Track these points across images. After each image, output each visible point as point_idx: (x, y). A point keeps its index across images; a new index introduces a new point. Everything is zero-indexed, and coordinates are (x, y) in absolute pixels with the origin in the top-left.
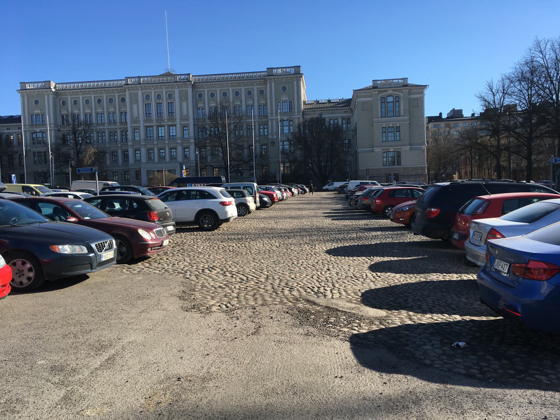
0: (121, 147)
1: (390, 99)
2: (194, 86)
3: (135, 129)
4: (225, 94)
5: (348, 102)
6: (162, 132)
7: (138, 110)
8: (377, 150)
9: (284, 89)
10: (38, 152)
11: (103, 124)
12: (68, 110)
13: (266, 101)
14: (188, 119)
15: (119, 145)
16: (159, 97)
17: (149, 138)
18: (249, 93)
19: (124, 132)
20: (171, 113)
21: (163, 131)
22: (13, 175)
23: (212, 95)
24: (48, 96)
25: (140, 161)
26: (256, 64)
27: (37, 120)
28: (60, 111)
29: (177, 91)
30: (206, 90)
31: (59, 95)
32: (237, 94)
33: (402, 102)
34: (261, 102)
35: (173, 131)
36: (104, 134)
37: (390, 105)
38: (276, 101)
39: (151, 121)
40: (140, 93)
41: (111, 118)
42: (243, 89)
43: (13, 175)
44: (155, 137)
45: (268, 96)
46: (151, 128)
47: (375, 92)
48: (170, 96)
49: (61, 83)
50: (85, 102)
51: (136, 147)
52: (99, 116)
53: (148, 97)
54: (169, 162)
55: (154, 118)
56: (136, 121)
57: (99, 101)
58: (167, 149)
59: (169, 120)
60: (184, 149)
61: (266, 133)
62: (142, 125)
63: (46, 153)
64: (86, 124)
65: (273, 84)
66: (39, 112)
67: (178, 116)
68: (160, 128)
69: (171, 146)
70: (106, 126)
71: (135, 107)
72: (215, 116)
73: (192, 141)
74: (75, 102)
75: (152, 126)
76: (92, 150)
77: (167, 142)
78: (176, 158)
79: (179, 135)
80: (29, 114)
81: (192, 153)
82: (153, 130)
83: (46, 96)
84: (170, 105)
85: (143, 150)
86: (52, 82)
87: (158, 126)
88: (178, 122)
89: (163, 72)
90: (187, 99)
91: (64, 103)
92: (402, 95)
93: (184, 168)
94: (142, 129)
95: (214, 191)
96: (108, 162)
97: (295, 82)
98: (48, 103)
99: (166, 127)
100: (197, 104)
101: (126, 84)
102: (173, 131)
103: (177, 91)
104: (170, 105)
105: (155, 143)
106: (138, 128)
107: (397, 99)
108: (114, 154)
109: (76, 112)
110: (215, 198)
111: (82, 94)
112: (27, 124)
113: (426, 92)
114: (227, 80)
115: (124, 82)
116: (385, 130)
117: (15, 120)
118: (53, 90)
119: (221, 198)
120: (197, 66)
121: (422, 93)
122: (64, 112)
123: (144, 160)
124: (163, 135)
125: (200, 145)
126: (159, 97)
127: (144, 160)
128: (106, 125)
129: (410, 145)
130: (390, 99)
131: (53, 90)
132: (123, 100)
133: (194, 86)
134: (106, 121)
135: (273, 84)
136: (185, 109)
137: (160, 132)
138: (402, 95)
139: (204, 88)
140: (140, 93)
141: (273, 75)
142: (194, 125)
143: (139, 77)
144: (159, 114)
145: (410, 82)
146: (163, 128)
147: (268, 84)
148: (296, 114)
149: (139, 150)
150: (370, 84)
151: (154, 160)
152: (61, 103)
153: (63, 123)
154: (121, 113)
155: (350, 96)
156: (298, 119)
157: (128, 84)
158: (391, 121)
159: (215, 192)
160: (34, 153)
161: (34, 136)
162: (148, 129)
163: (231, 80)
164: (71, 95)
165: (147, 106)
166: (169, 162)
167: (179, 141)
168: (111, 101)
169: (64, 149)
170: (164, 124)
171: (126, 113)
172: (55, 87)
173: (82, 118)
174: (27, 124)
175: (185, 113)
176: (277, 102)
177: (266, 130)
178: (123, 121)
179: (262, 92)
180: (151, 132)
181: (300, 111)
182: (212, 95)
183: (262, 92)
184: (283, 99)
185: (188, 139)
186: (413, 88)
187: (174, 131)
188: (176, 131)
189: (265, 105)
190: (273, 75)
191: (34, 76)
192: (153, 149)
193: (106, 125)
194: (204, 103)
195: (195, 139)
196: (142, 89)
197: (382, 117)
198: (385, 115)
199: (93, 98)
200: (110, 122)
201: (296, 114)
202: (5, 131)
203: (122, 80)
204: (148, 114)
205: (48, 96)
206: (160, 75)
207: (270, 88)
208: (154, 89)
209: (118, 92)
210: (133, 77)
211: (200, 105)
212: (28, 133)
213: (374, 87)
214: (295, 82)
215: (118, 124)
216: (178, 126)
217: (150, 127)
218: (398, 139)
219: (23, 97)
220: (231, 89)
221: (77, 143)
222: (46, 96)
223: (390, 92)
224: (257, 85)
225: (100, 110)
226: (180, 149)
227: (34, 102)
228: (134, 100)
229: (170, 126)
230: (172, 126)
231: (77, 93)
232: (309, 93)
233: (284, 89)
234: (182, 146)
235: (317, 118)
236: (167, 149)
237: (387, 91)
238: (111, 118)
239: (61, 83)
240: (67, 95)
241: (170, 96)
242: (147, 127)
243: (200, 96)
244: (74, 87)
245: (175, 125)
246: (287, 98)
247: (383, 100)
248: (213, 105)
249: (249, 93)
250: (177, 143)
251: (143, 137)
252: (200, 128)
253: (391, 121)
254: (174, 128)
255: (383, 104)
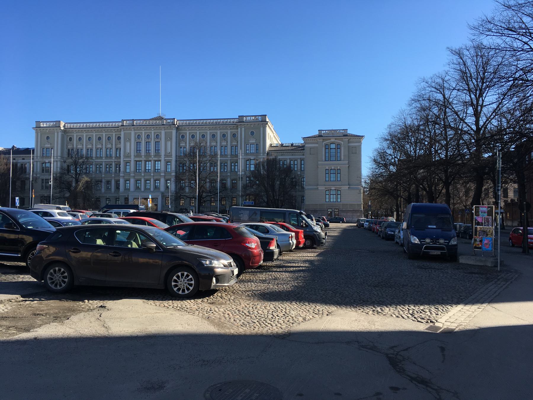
0: (115, 177)
1: (333, 146)
2: (178, 129)
3: (127, 163)
4: (203, 136)
5: (301, 148)
6: (149, 166)
7: (130, 147)
8: (321, 188)
9: (252, 133)
10: (46, 180)
11: (101, 158)
12: (73, 145)
13: (237, 142)
14: (171, 156)
15: (113, 175)
16: (148, 136)
17: (138, 171)
18: (224, 136)
19: (118, 165)
20: (157, 151)
21: (150, 165)
22: (17, 198)
23: (193, 136)
24: (58, 133)
25: (129, 189)
26: (229, 111)
27: (46, 152)
28: (67, 146)
29: (163, 132)
30: (188, 132)
31: (68, 133)
32: (214, 136)
33: (342, 149)
34: (234, 144)
35: (158, 166)
36: (91, 166)
37: (333, 151)
38: (245, 143)
39: (141, 156)
40: (133, 133)
41: (108, 153)
42: (219, 132)
43: (17, 198)
44: (143, 170)
45: (239, 139)
46: (140, 163)
47: (320, 140)
48: (157, 136)
49: (69, 123)
50: (87, 139)
51: (126, 178)
52: (108, 150)
53: (139, 137)
54: (143, 192)
55: (143, 154)
56: (129, 156)
57: (100, 139)
58: (152, 180)
59: (155, 156)
60: (167, 180)
61: (236, 170)
62: (133, 159)
63: (48, 181)
64: (87, 158)
65: (243, 129)
66: (49, 146)
67: (163, 153)
68: (147, 163)
69: (146, 177)
70: (104, 160)
71: (128, 144)
72: (192, 154)
73: (174, 174)
74: (80, 139)
75: (141, 161)
76: (85, 179)
77: (152, 174)
78: (159, 189)
79: (163, 169)
80: (41, 147)
81: (172, 186)
82: (141, 164)
83: (56, 134)
84: (157, 143)
85: (132, 181)
86: (62, 122)
87: (146, 161)
88: (162, 158)
89: (155, 116)
90: (171, 139)
91: (71, 139)
92: (342, 143)
93: (150, 197)
94: (132, 163)
95: (54, 213)
96: (103, 190)
97: (262, 129)
98: (57, 139)
99: (152, 162)
100: (179, 144)
101: (122, 126)
102: (158, 166)
103: (163, 132)
104: (157, 143)
105: (143, 175)
106: (129, 162)
107: (338, 147)
108: (108, 182)
109: (80, 147)
110: (53, 216)
111: (86, 133)
112: (39, 155)
113: (364, 142)
114: (206, 124)
115: (120, 124)
116: (328, 172)
117: (27, 151)
118: (62, 128)
119: (56, 216)
120: (181, 112)
121: (360, 142)
122: (70, 147)
123: (132, 188)
124: (150, 168)
125: (178, 179)
126: (148, 136)
127: (132, 188)
128: (104, 158)
129: (349, 185)
130: (333, 146)
131: (62, 128)
132: (119, 138)
133: (178, 129)
134: (104, 156)
135: (243, 129)
136: (169, 148)
137: (147, 165)
138: (342, 143)
139: (186, 130)
140: (133, 133)
141: (243, 122)
142: (176, 161)
143: (133, 120)
144: (148, 151)
145: (349, 132)
146: (150, 163)
147: (239, 129)
148: (262, 154)
149: (129, 180)
150: (317, 133)
151: (140, 189)
152: (68, 139)
153: (68, 156)
154: (117, 149)
155: (299, 141)
156: (262, 158)
157: (123, 126)
158: (333, 165)
159: (54, 213)
160: (43, 180)
161: (44, 165)
162: (138, 163)
163: (210, 124)
164: (76, 133)
165: (138, 144)
166: (143, 192)
167: (152, 174)
168: (109, 138)
169: (67, 178)
170: (141, 159)
171: (120, 149)
172: (64, 126)
173: (84, 152)
174: (39, 155)
175: (169, 150)
176: (246, 144)
177: (236, 167)
178: (118, 155)
179: (234, 135)
180: (140, 166)
181: (265, 153)
182: (193, 136)
183: (234, 135)
184: (251, 142)
185: (170, 173)
186: (352, 138)
187: (159, 165)
188: (160, 166)
189: (237, 146)
190: (243, 122)
191: (47, 117)
192: (140, 180)
193: (104, 158)
194: (186, 143)
195: (176, 173)
196: (134, 130)
197: (326, 160)
198: (328, 159)
199: (104, 136)
200: (107, 157)
201: (262, 154)
202: (19, 161)
203: (119, 122)
204: (138, 151)
205: (58, 133)
206: (152, 119)
207: (241, 132)
208: (145, 130)
209: (115, 132)
210: (128, 120)
211: (182, 144)
212: (39, 163)
213: (320, 136)
214: (262, 129)
215: (114, 158)
216: (163, 162)
217: (139, 161)
218: (339, 179)
219: (37, 133)
220: (208, 132)
221: (76, 174)
222: (56, 134)
223: (333, 140)
224: (231, 129)
225: (99, 146)
226: (162, 180)
227: (46, 138)
228: (128, 139)
229: (155, 161)
230: (158, 161)
231: (82, 132)
232: (272, 138)
233: (252, 133)
234: (165, 178)
235: (273, 159)
236: (152, 180)
237: (330, 139)
238: (108, 153)
239: (69, 123)
240: (73, 133)
241: (157, 136)
242: (137, 161)
243: (183, 136)
244: (99, 126)
245: (160, 161)
246: (254, 141)
247: (327, 147)
248: (192, 144)
249: (224, 136)
250: (161, 176)
251: (132, 169)
252: (180, 164)
253: (333, 165)
254: (159, 162)
255: (327, 150)
